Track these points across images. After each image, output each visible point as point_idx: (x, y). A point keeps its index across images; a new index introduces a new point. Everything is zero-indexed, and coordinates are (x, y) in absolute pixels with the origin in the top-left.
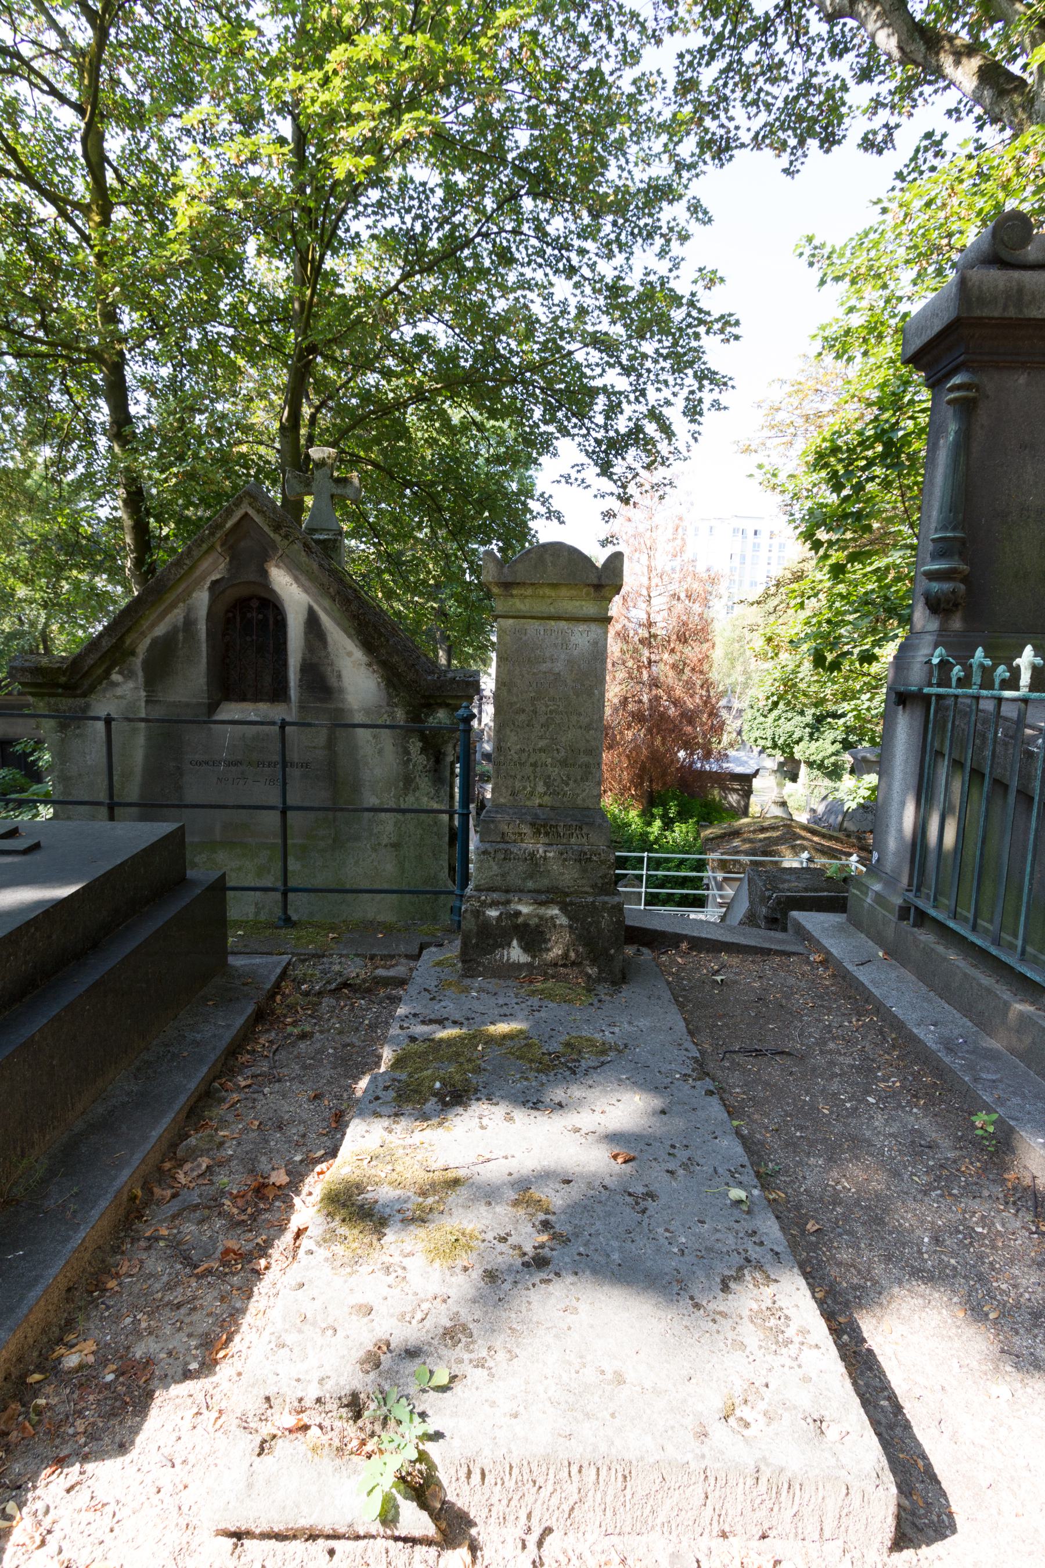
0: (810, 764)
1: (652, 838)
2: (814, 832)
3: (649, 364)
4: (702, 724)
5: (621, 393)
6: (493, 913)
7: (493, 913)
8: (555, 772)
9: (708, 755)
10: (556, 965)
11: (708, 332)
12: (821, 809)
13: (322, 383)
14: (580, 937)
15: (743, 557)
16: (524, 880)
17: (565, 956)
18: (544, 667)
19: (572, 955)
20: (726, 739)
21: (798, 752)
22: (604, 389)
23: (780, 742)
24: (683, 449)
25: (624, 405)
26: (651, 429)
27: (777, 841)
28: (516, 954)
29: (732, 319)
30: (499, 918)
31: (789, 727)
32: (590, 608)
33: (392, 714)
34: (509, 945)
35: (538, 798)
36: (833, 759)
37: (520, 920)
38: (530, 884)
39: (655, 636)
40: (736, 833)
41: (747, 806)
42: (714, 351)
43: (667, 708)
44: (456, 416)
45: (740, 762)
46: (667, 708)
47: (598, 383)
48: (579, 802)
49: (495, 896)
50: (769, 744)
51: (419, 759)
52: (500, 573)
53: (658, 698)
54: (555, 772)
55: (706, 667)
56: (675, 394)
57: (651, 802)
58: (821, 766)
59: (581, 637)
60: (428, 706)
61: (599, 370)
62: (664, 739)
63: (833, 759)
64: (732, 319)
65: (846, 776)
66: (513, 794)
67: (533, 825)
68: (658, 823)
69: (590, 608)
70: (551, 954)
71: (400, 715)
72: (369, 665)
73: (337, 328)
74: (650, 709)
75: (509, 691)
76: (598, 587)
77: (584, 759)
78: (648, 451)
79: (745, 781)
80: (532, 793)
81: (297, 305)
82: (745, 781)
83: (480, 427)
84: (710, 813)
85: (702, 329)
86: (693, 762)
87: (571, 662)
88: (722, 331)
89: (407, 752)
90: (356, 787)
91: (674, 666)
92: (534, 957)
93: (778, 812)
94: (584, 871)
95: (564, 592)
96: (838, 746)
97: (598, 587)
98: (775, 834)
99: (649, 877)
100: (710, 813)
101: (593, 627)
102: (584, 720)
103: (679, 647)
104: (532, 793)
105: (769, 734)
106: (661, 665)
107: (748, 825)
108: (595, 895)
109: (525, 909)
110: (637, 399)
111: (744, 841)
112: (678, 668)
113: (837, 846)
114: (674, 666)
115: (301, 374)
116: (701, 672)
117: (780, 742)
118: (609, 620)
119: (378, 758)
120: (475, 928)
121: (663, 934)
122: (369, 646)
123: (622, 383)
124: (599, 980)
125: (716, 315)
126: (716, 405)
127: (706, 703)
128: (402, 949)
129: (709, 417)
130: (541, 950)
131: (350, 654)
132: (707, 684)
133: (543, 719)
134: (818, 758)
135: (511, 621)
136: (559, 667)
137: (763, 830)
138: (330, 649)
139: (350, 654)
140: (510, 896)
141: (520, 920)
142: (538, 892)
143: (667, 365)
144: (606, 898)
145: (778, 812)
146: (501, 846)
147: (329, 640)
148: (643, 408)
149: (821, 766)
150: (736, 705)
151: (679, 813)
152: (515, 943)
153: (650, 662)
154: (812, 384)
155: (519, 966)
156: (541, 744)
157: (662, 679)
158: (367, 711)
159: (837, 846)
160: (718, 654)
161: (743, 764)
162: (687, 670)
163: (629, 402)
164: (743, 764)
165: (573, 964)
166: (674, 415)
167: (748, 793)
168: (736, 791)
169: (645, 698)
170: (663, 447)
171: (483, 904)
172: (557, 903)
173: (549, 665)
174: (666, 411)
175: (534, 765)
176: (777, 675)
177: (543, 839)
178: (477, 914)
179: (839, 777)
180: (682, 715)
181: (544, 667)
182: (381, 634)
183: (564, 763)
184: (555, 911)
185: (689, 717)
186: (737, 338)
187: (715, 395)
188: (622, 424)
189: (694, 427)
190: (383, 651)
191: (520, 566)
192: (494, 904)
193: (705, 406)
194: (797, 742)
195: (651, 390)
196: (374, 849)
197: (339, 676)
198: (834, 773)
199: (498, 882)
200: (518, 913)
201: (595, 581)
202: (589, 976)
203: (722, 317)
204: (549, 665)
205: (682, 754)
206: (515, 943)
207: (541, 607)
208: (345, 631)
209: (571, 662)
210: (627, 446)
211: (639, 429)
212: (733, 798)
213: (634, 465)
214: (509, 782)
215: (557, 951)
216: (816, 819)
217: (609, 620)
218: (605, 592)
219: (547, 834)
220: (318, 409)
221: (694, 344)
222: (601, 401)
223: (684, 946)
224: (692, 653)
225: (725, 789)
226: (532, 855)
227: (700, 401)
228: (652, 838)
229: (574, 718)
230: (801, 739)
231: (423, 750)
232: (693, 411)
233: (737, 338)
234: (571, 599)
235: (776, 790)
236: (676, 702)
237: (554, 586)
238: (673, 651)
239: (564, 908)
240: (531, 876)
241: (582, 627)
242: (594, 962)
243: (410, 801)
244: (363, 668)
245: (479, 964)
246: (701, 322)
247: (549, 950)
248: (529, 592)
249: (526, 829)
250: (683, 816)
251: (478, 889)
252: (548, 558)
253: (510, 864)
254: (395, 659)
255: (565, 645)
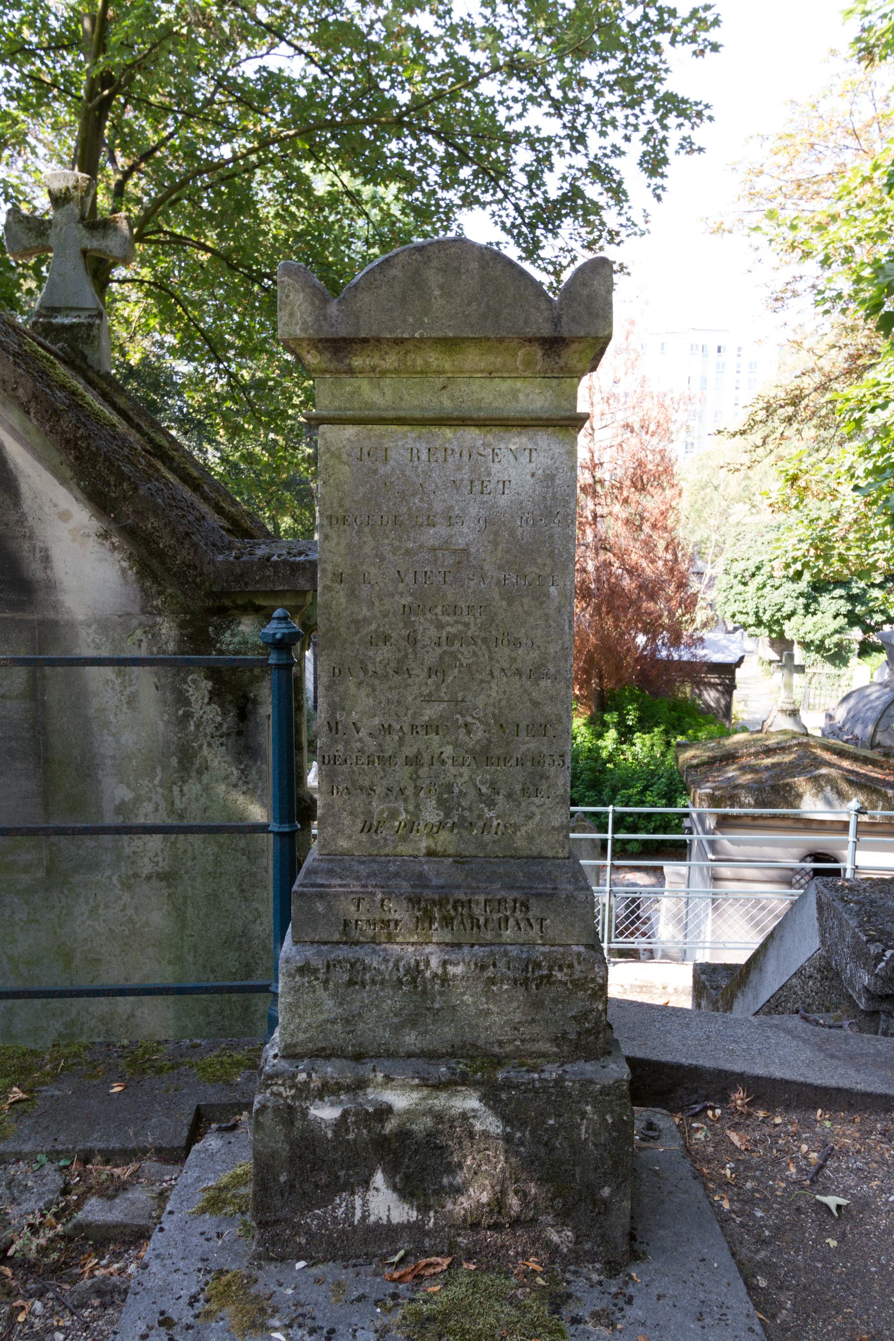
0: (806, 646)
1: (604, 754)
2: (841, 753)
3: (588, 97)
4: (669, 600)
5: (549, 139)
6: (326, 1113)
7: (326, 1113)
8: (463, 776)
9: (676, 640)
10: (475, 1226)
11: (673, 42)
12: (840, 715)
13: (129, 139)
14: (529, 1163)
15: (704, 381)
16: (397, 1029)
17: (499, 1204)
18: (431, 536)
19: (514, 1202)
20: (700, 616)
21: (791, 630)
22: (527, 133)
23: (766, 618)
24: (638, 219)
25: (555, 158)
26: (593, 191)
27: (794, 769)
28: (382, 1203)
29: (710, 16)
30: (341, 1124)
31: (776, 597)
32: (533, 397)
33: (151, 631)
34: (366, 1183)
35: (426, 836)
36: (836, 638)
37: (390, 1126)
38: (411, 1039)
39: (601, 482)
40: (730, 757)
41: (728, 707)
42: (682, 71)
43: (619, 578)
44: (321, 185)
45: (718, 648)
46: (619, 578)
47: (518, 126)
48: (520, 842)
49: (330, 1070)
50: (751, 620)
51: (207, 713)
52: (321, 316)
53: (608, 565)
54: (463, 776)
55: (670, 523)
56: (627, 138)
57: (603, 704)
58: (820, 647)
59: (515, 464)
60: (221, 611)
61: (517, 108)
62: (617, 619)
63: (836, 638)
64: (710, 16)
65: (854, 660)
66: (367, 828)
67: (414, 901)
68: (612, 734)
69: (533, 397)
70: (465, 1202)
71: (167, 628)
72: (104, 536)
73: (141, 47)
74: (598, 580)
75: (352, 594)
76: (553, 344)
77: (528, 745)
78: (588, 223)
79: (726, 672)
80: (411, 826)
81: (87, 24)
82: (726, 672)
83: (354, 197)
84: (681, 718)
85: (664, 39)
86: (655, 650)
87: (492, 524)
88: (693, 39)
89: (182, 700)
90: (87, 769)
91: (627, 522)
92: (424, 1209)
93: (787, 724)
94: (537, 1004)
95: (472, 358)
96: (842, 621)
97: (553, 344)
98: (787, 758)
99: (615, 841)
100: (681, 718)
101: (544, 440)
102: (528, 657)
103: (634, 497)
104: (411, 826)
105: (751, 607)
106: (610, 520)
107: (746, 744)
108: (562, 1060)
109: (400, 1100)
110: (574, 148)
111: (743, 769)
112: (634, 524)
113: (876, 774)
114: (627, 522)
115: (94, 115)
116: (665, 528)
117: (766, 618)
118: (577, 421)
119: (128, 717)
120: (284, 1149)
121: (694, 1073)
122: (99, 500)
123: (552, 127)
124: (577, 1257)
125: (684, 12)
126: (688, 146)
127: (672, 570)
128: (150, 1139)
129: (678, 163)
130: (440, 1191)
131: (65, 516)
132: (672, 545)
133: (431, 657)
134: (816, 637)
135: (350, 431)
136: (465, 534)
137: (769, 751)
138: (27, 505)
139: (65, 516)
140: (365, 1070)
141: (390, 1126)
142: (431, 1056)
143: (614, 98)
144: (589, 1068)
145: (787, 724)
146: (344, 952)
147: (24, 488)
148: (581, 162)
149: (820, 647)
150: (709, 572)
151: (640, 720)
152: (379, 1179)
153: (595, 517)
154: (803, 137)
155: (389, 1232)
156: (430, 713)
157: (612, 540)
158: (104, 625)
159: (876, 774)
160: (684, 505)
161: (721, 649)
162: (646, 528)
163: (562, 154)
164: (721, 649)
165: (516, 1222)
166: (628, 169)
167: (729, 688)
168: (713, 686)
169: (590, 567)
170: (611, 218)
171: (303, 1091)
172: (475, 1085)
173: (442, 530)
174: (614, 162)
175: (415, 761)
176: (803, 531)
177: (438, 934)
178: (289, 1114)
179: (845, 662)
180: (640, 587)
181: (431, 536)
182: (122, 477)
183: (483, 756)
184: (469, 1102)
185: (651, 589)
186: (715, 48)
187: (686, 131)
188: (554, 186)
189: (658, 180)
190: (127, 509)
191: (365, 298)
192: (327, 1091)
193: (670, 151)
194: (789, 617)
195: (592, 136)
196: (127, 886)
197: (46, 559)
198: (838, 657)
199: (338, 1035)
200: (384, 1112)
201: (546, 331)
202: (554, 1250)
203: (695, 11)
204: (442, 530)
205: (641, 639)
206: (379, 1179)
207: (418, 397)
208: (55, 473)
209: (492, 524)
210: (560, 217)
211: (576, 192)
212: (711, 696)
213: (572, 244)
214: (359, 803)
215: (480, 1194)
216: (834, 731)
217: (577, 421)
218: (572, 356)
219: (447, 921)
220: (127, 175)
221: (652, 59)
222: (523, 156)
223: (739, 1098)
224: (652, 503)
225: (699, 683)
226: (415, 972)
227: (664, 140)
228: (604, 754)
229: (504, 652)
230: (793, 613)
231: (215, 696)
232: (654, 164)
233: (715, 48)
234: (490, 375)
235: (783, 693)
236: (632, 571)
237: (450, 344)
238: (626, 501)
239: (491, 1096)
240: (413, 1021)
241: (517, 441)
242: (564, 1217)
243: (191, 799)
244: (92, 543)
245: (296, 1228)
246: (662, 28)
247: (459, 1190)
248: (391, 361)
249: (398, 911)
250: (645, 724)
251: (290, 1054)
252: (433, 277)
253: (363, 996)
254: (151, 523)
255: (478, 483)
